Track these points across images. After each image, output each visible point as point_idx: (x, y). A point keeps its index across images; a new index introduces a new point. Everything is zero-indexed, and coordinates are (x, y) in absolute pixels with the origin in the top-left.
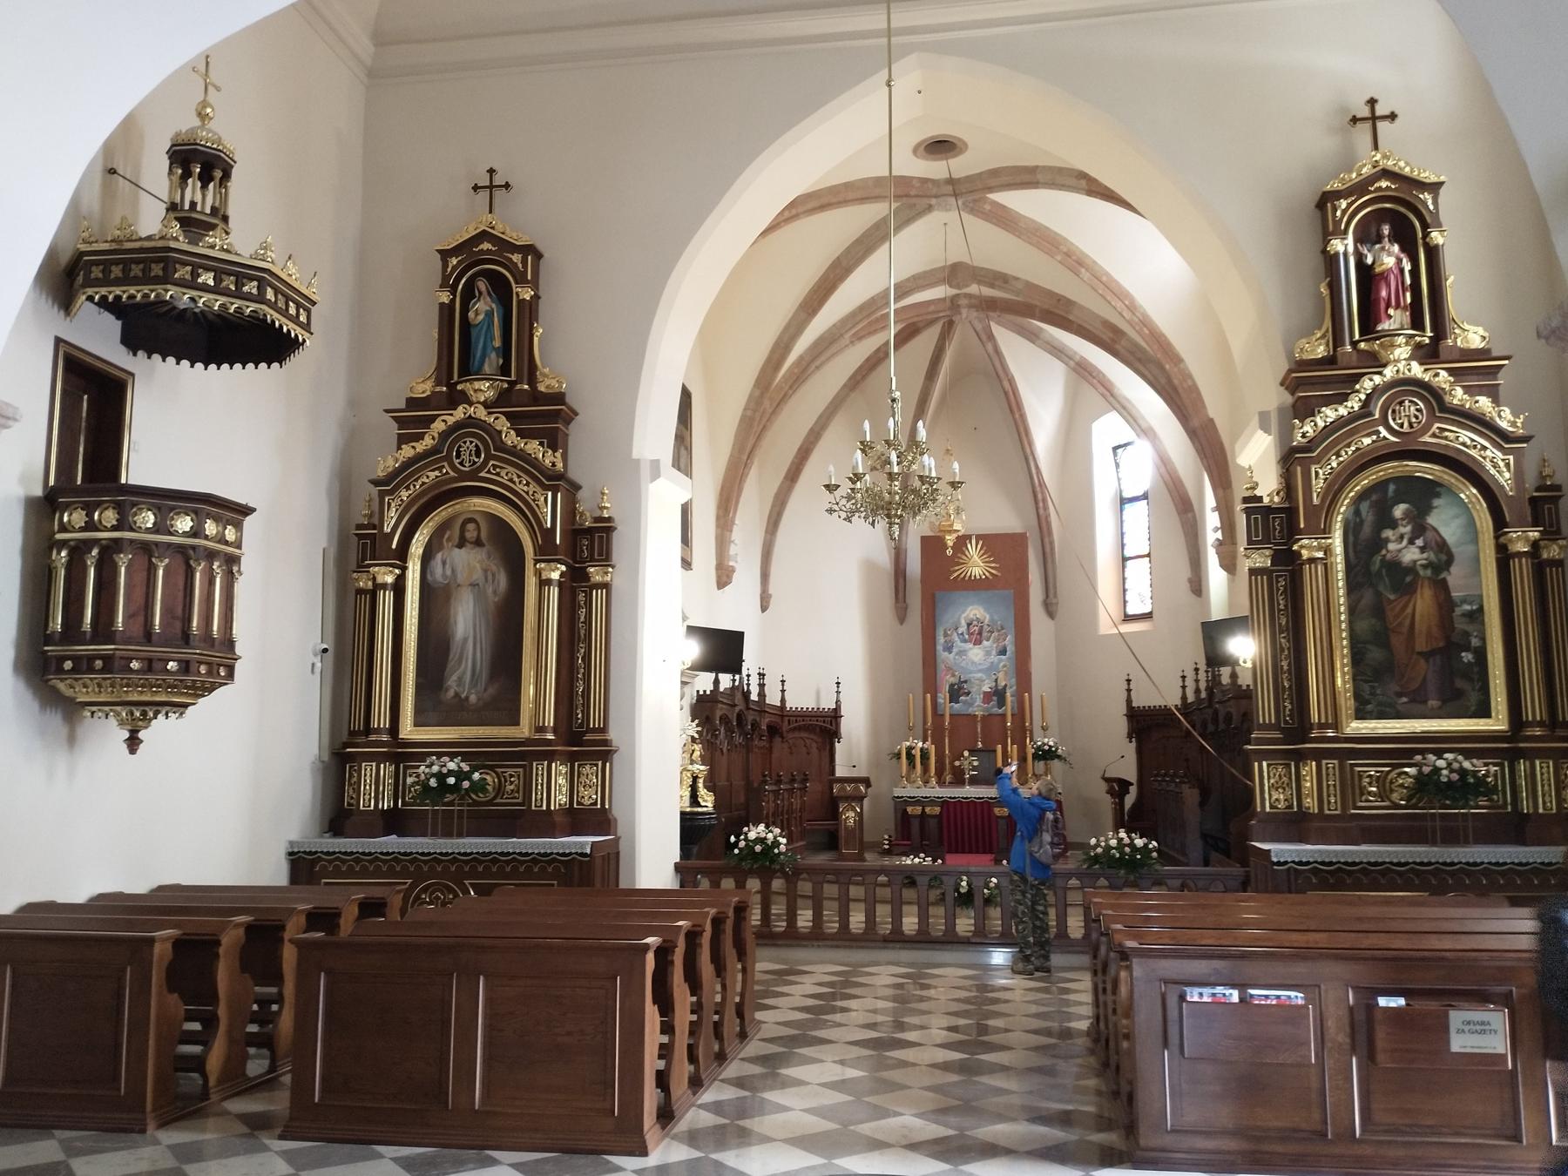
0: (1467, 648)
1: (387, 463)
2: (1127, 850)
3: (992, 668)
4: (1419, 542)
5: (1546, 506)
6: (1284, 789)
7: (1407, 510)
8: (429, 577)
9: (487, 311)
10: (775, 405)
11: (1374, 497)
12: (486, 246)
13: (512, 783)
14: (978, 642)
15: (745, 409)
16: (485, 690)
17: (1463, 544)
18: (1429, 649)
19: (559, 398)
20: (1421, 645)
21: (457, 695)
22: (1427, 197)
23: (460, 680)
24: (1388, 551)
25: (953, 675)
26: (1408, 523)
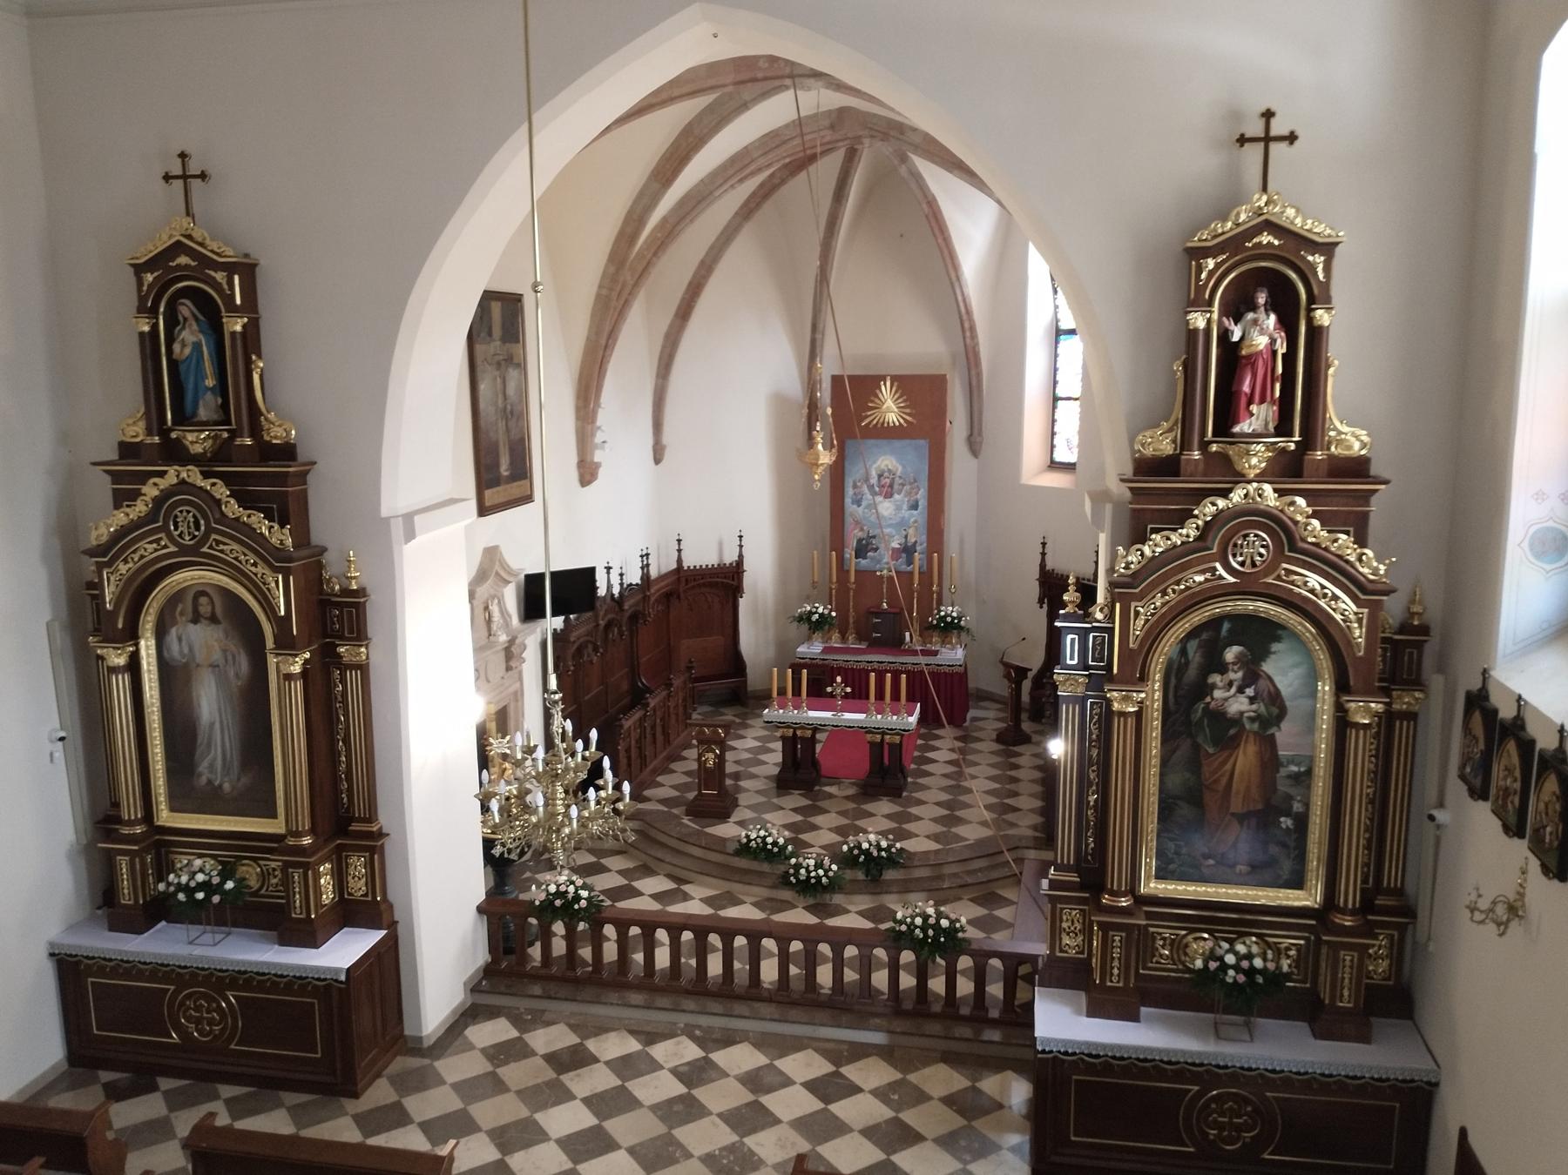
0: (1288, 814)
1: (100, 533)
2: (931, 932)
3: (902, 524)
4: (1250, 691)
5: (1408, 650)
6: (1076, 935)
7: (1241, 653)
8: (166, 654)
9: (193, 343)
10: (637, 276)
11: (1204, 636)
12: (183, 260)
13: (275, 877)
14: (889, 495)
15: (600, 287)
16: (239, 779)
17: (1301, 697)
18: (1245, 810)
19: (287, 452)
20: (1237, 805)
21: (210, 782)
22: (1319, 260)
23: (211, 767)
24: (1213, 699)
25: (862, 530)
26: (1239, 668)
